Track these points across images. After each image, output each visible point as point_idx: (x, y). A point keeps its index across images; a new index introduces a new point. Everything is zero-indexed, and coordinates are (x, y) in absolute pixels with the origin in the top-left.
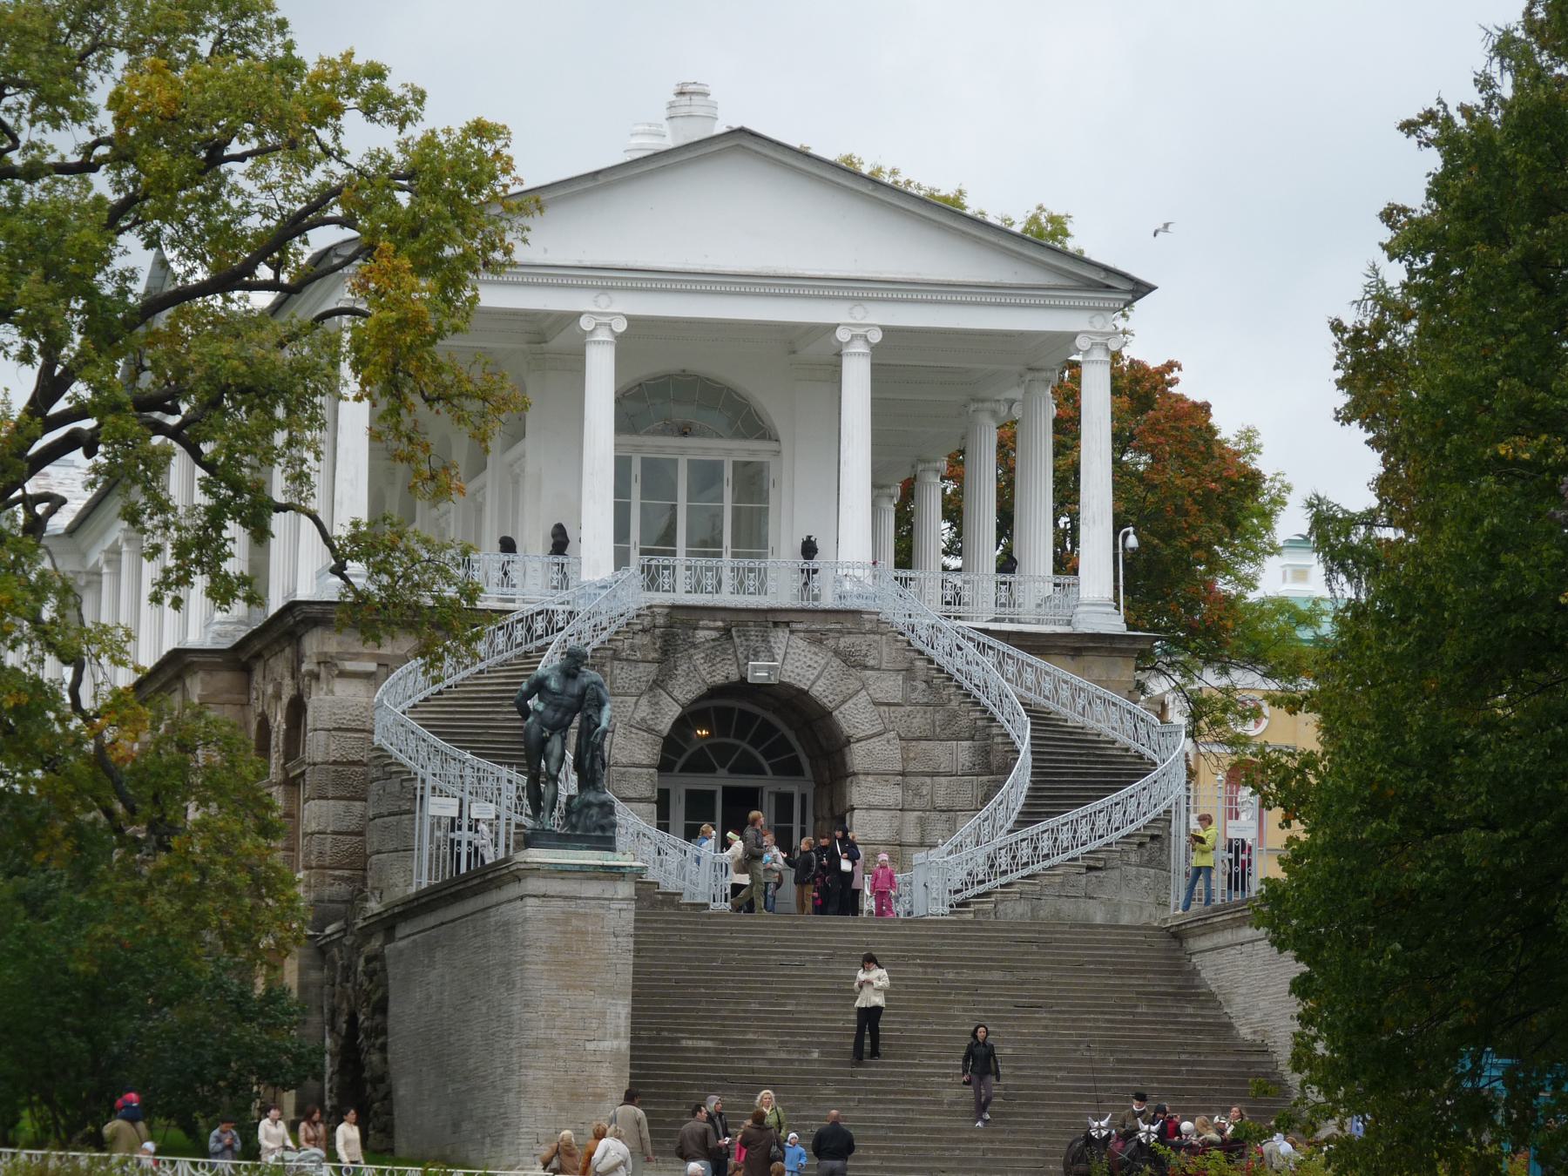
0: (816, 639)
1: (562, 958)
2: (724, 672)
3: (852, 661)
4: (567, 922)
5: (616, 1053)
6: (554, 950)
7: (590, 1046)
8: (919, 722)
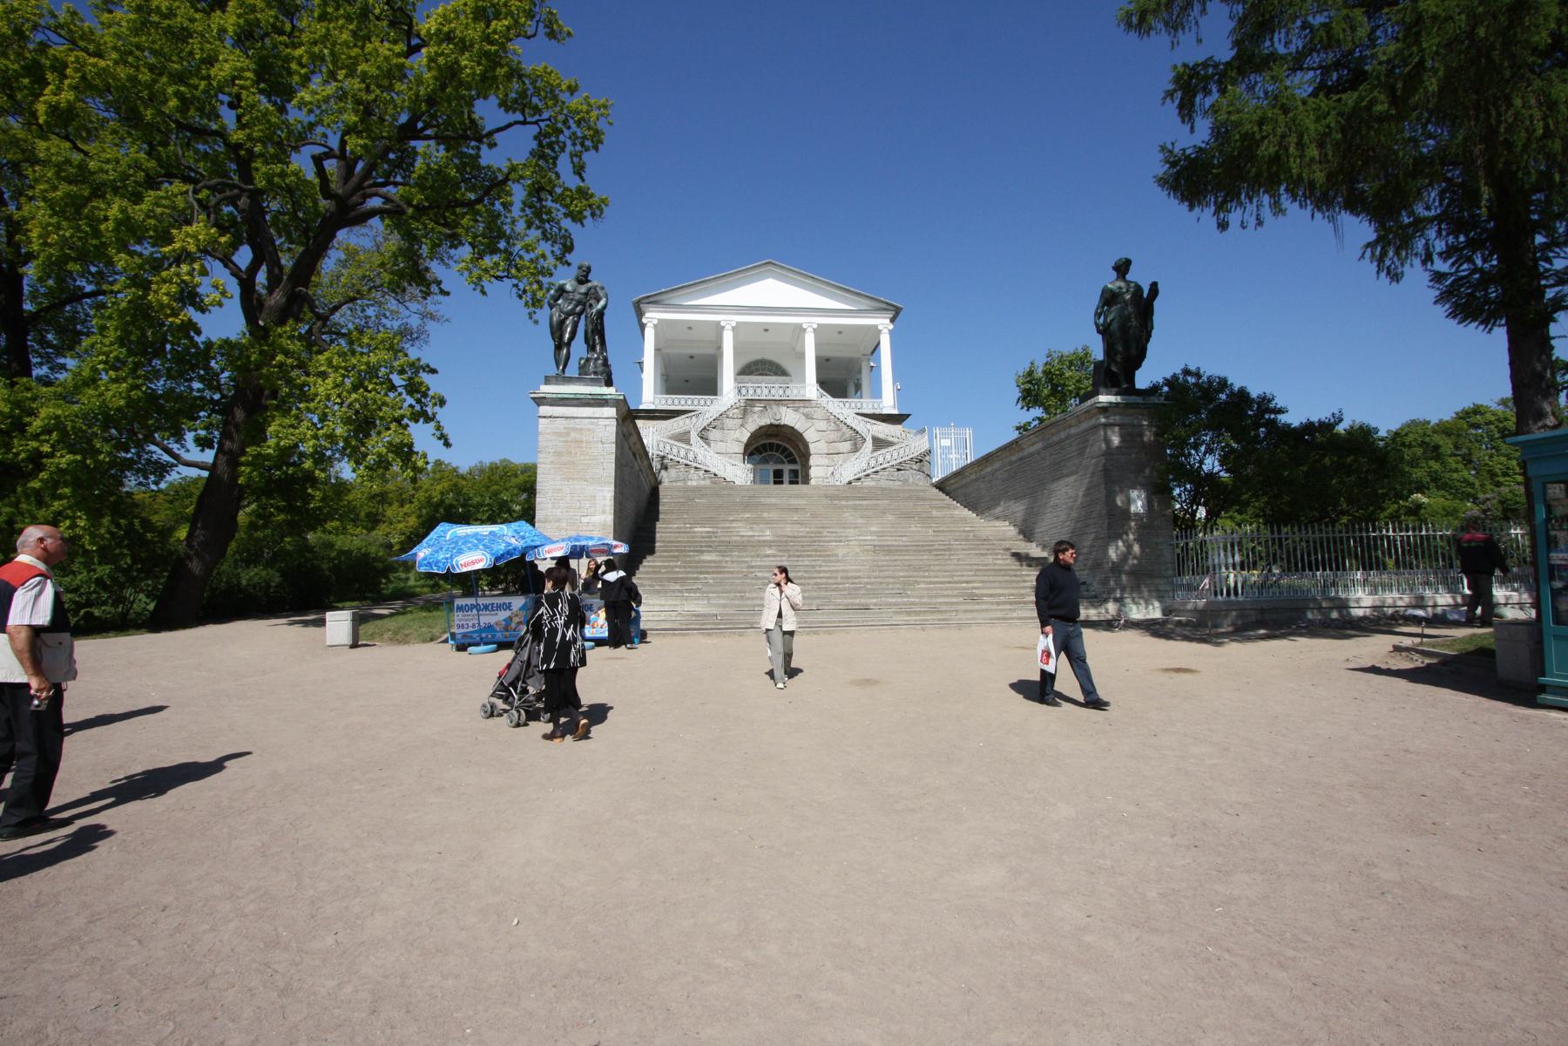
0: (796, 409)
1: (566, 459)
2: (766, 421)
3: (808, 416)
4: (567, 434)
5: (604, 526)
6: (558, 454)
7: (584, 520)
8: (833, 436)
